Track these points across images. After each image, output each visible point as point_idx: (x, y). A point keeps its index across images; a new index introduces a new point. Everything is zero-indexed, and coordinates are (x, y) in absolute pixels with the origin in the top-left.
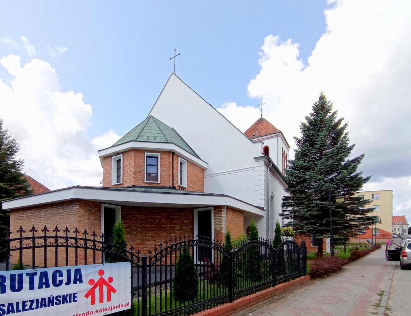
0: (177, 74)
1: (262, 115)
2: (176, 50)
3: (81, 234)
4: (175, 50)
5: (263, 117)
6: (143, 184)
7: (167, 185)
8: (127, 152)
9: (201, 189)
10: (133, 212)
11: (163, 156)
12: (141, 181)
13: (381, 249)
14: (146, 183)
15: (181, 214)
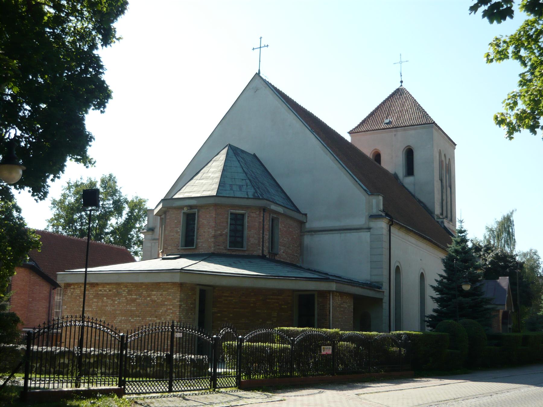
1: (402, 82)
2: (262, 39)
3: (73, 318)
4: (261, 38)
5: (405, 86)
6: (225, 251)
7: (255, 253)
12: (223, 248)
13: (397, 172)
15: (279, 297)
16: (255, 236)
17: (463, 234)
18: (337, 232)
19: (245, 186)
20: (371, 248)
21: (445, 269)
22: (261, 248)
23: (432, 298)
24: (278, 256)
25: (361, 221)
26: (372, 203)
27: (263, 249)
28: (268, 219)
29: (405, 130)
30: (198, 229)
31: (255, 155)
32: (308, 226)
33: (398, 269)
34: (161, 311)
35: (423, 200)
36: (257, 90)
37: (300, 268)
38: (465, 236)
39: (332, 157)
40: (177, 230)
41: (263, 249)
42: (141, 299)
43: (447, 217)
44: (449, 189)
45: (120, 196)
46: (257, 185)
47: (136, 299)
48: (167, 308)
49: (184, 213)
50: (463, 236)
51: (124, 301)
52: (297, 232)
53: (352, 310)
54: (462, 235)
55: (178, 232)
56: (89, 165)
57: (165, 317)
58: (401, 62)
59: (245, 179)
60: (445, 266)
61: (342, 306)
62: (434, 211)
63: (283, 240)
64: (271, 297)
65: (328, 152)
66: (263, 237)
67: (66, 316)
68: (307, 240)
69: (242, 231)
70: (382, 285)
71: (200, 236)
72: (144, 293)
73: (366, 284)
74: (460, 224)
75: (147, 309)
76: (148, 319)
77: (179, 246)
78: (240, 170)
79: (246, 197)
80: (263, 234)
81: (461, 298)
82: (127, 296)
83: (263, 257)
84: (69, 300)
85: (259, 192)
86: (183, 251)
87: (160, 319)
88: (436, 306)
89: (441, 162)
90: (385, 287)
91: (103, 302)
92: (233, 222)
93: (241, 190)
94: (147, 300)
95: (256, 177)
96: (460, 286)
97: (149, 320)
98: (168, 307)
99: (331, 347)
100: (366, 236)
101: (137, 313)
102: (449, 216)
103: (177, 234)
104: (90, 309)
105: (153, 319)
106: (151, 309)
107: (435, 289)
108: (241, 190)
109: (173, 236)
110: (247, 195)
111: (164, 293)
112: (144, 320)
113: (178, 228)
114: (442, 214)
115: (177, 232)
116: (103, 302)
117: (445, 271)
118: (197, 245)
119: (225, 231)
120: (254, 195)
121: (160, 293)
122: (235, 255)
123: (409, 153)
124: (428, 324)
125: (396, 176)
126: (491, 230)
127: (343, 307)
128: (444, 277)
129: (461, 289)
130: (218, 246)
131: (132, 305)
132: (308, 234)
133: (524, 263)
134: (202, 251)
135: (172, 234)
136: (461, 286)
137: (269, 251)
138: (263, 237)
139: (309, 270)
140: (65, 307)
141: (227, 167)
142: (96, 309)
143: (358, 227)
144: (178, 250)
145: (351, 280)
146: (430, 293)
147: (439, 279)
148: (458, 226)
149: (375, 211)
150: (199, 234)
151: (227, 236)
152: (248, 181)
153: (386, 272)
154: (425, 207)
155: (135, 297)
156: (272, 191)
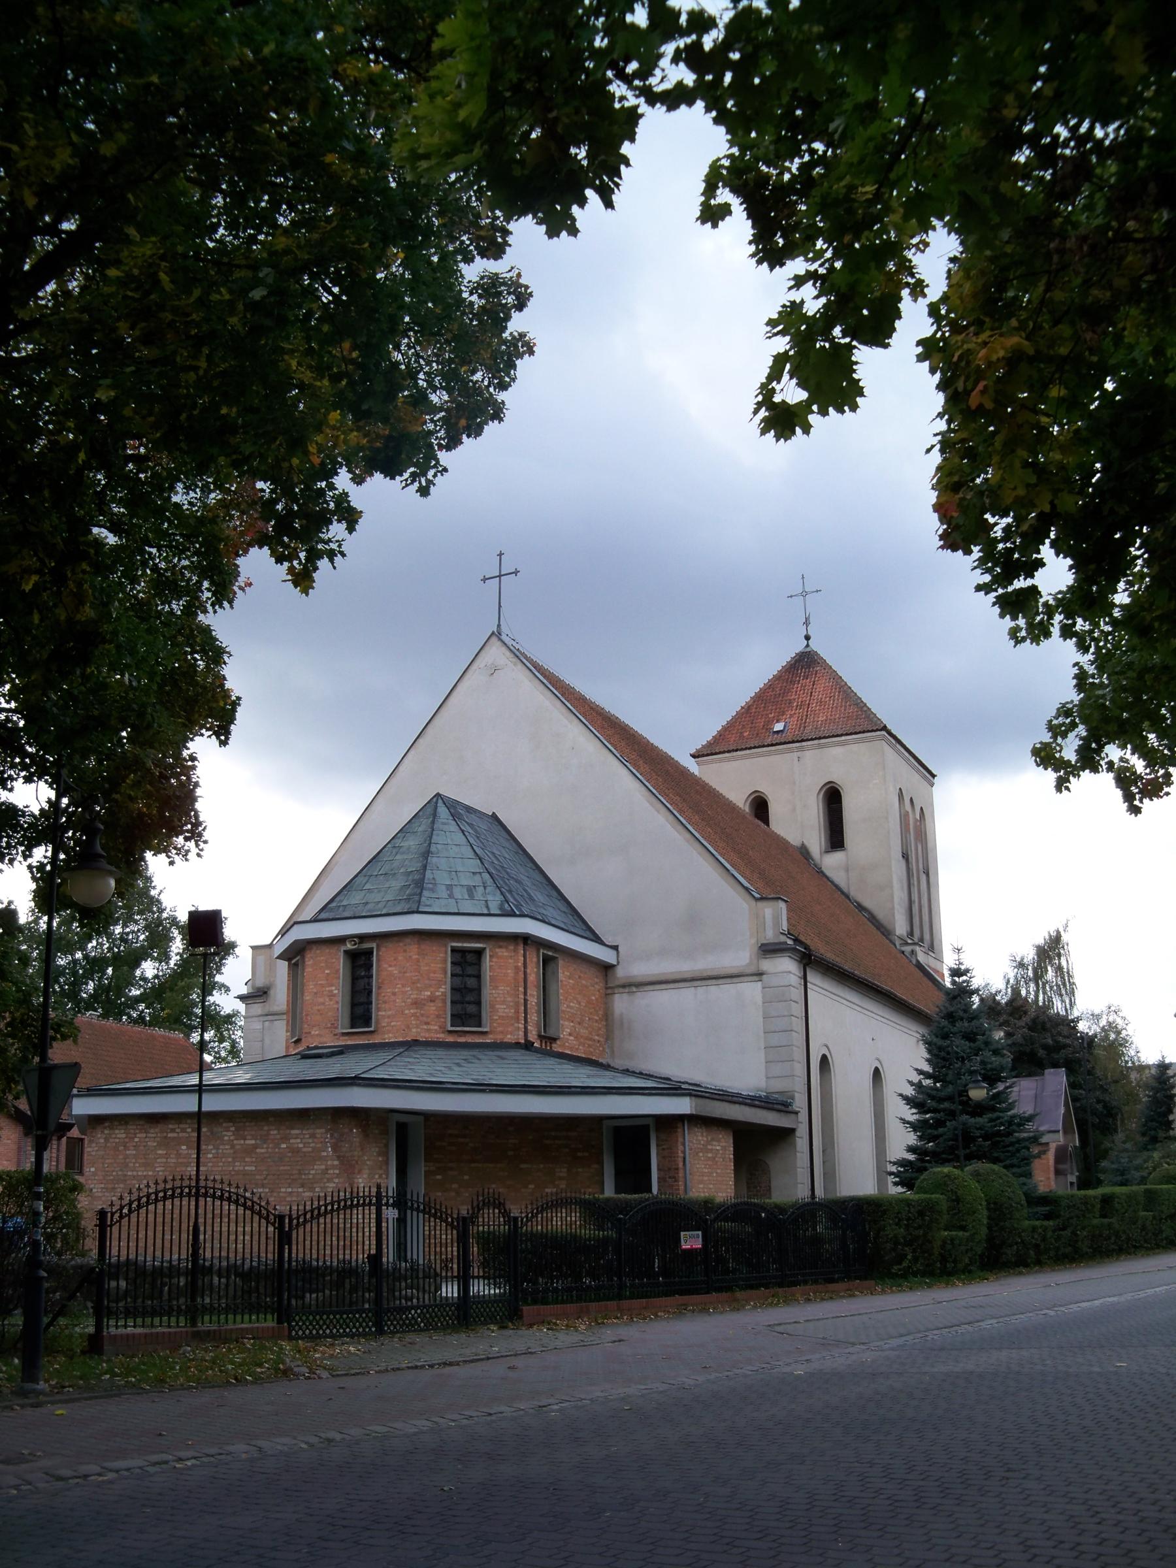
0: (504, 637)
4: (501, 555)
5: (814, 645)
6: (442, 1035)
7: (509, 1038)
8: (395, 938)
9: (598, 1035)
10: (450, 1132)
11: (497, 950)
12: (436, 1027)
13: (806, 843)
14: (450, 1032)
16: (509, 999)
17: (964, 978)
18: (687, 984)
19: (482, 888)
20: (766, 1017)
21: (928, 1056)
22: (521, 1026)
23: (904, 1121)
24: (558, 1042)
25: (741, 957)
26: (764, 918)
27: (526, 1028)
28: (535, 960)
29: (820, 747)
30: (379, 988)
31: (494, 816)
32: (621, 973)
33: (824, 1060)
34: (313, 1172)
35: (867, 903)
36: (494, 670)
37: (607, 1067)
38: (968, 982)
39: (671, 817)
40: (332, 991)
41: (526, 1028)
42: (267, 1148)
43: (922, 940)
44: (923, 878)
45: (161, 911)
46: (506, 884)
47: (255, 1147)
48: (326, 1165)
49: (345, 952)
50: (964, 982)
51: (228, 1151)
52: (597, 987)
53: (732, 1156)
54: (962, 979)
55: (334, 995)
56: (177, 859)
57: (322, 1185)
58: (804, 594)
59: (480, 873)
60: (929, 1051)
61: (709, 1147)
62: (895, 929)
63: (568, 1006)
64: (553, 1134)
65: (660, 805)
66: (526, 1001)
67: (171, 1178)
68: (621, 1003)
69: (478, 990)
70: (793, 1098)
71: (385, 1002)
72: (272, 1132)
73: (753, 1098)
74: (956, 957)
75: (282, 1168)
76: (283, 1190)
77: (336, 1028)
78: (468, 852)
79: (486, 912)
80: (525, 993)
81: (965, 1117)
82: (235, 1142)
83: (528, 1046)
84: (102, 1153)
85: (512, 900)
86: (346, 1038)
87: (312, 1189)
88: (912, 1139)
89: (904, 818)
90: (800, 1103)
91: (178, 1155)
92: (458, 970)
93: (471, 897)
94: (280, 1148)
95: (503, 867)
96: (964, 1092)
97: (285, 1192)
98: (329, 1163)
99: (700, 1233)
100: (752, 991)
101: (258, 1177)
102: (927, 937)
103: (331, 1000)
104: (150, 1173)
105: (295, 1190)
106: (289, 1168)
107: (908, 1100)
108: (471, 897)
109: (323, 1004)
110: (487, 907)
111: (318, 1131)
112: (275, 1194)
113: (332, 986)
114: (911, 934)
115: (331, 996)
116: (178, 1155)
117: (927, 1060)
118: (377, 1022)
119: (442, 990)
120: (501, 907)
121: (311, 1131)
122: (466, 1043)
123: (833, 798)
124: (897, 1179)
125: (804, 852)
126: (1021, 965)
127: (712, 1149)
128: (927, 1075)
129: (965, 1098)
130: (427, 1023)
131: (247, 1159)
132: (621, 990)
133: (1095, 1035)
134: (389, 1038)
135: (321, 1000)
136: (967, 1092)
137: (539, 1031)
138: (526, 1001)
139: (627, 1072)
140: (93, 1169)
141: (438, 846)
142: (163, 1171)
143: (734, 971)
144: (335, 1035)
145: (722, 1091)
146: (899, 1111)
147: (916, 1078)
148: (949, 960)
149: (770, 936)
150: (381, 998)
151: (444, 1001)
152: (486, 876)
153: (800, 1070)
154: (873, 919)
155: (253, 1142)
156: (539, 897)
